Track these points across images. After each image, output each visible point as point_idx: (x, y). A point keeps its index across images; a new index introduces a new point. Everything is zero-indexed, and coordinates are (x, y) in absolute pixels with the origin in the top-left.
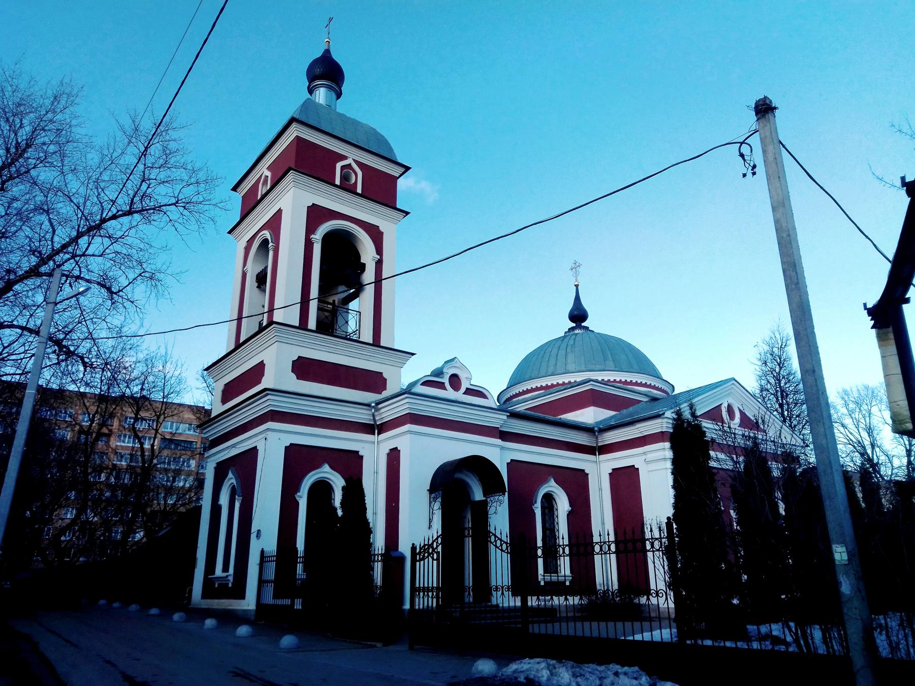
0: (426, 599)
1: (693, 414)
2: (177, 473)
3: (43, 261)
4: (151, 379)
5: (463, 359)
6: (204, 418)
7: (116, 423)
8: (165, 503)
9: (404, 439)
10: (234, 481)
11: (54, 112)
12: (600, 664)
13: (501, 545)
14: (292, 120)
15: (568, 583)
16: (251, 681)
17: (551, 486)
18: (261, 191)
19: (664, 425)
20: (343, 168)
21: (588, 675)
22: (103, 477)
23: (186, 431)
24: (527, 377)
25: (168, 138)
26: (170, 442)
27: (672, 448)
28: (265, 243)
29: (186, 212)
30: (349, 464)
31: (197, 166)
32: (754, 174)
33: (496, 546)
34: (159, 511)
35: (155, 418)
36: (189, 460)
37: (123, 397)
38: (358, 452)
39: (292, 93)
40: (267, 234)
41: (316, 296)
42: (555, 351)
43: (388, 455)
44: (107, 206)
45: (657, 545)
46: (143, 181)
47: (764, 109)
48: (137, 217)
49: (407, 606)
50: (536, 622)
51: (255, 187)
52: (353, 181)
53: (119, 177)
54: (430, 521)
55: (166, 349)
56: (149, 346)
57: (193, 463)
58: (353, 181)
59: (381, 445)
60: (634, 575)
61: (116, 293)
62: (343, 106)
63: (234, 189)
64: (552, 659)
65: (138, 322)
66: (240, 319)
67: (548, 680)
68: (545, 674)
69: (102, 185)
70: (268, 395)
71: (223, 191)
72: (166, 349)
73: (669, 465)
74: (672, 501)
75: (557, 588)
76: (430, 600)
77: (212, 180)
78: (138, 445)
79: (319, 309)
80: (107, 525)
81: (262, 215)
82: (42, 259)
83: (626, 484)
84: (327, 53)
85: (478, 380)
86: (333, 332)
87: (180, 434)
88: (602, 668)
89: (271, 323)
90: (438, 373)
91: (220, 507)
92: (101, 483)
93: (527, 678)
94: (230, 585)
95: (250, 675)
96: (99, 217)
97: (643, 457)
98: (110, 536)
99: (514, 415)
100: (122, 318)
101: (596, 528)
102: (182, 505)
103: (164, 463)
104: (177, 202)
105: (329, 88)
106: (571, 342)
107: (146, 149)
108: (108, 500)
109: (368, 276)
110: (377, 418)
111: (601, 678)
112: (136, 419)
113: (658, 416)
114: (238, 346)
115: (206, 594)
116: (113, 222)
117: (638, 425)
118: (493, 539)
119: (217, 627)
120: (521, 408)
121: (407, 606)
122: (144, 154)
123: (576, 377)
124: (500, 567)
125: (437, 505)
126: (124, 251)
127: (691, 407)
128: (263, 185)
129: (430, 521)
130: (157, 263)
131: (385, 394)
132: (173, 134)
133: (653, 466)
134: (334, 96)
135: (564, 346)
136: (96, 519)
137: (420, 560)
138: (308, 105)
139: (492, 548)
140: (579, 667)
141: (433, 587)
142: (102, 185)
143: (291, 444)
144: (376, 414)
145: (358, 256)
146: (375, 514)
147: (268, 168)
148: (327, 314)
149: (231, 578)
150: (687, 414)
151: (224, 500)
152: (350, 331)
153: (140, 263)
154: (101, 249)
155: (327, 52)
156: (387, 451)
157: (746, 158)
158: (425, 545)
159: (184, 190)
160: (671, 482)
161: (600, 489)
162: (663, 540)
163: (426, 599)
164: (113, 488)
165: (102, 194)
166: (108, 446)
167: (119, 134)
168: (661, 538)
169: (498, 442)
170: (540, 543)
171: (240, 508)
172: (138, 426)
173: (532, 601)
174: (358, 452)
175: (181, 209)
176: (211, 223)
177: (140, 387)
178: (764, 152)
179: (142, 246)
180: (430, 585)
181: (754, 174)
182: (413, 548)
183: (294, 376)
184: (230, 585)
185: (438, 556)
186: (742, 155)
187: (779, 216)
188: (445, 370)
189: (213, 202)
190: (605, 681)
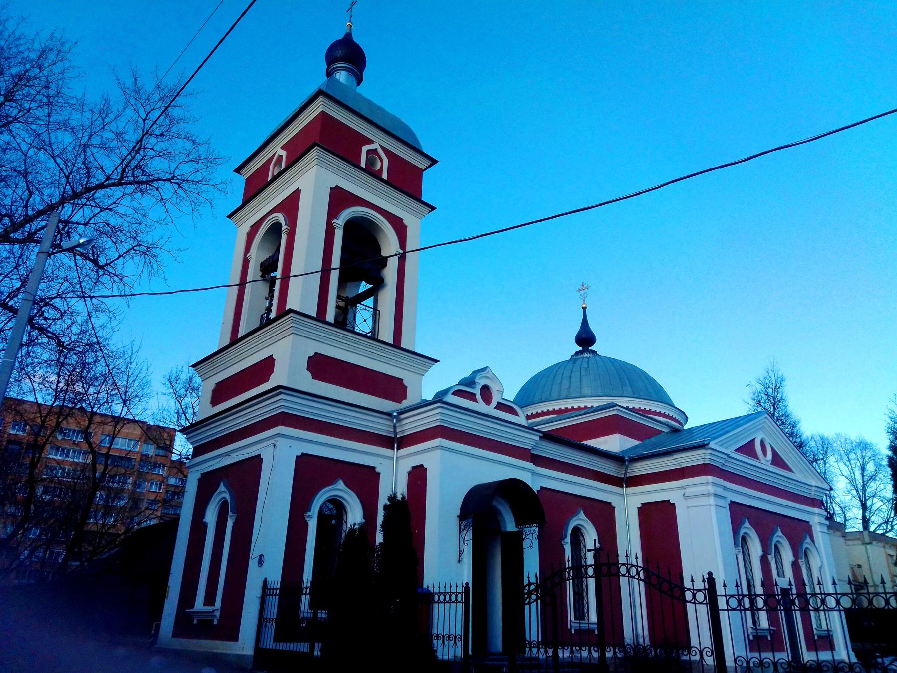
3: (16, 227)
5: (495, 370)
9: (433, 457)
10: (227, 496)
11: (41, 68)
14: (320, 93)
17: (581, 520)
18: (272, 171)
20: (369, 152)
24: (537, 399)
28: (275, 229)
29: (180, 191)
38: (639, 509)
40: (280, 217)
42: (567, 374)
43: (410, 473)
48: (129, 189)
52: (378, 167)
54: (461, 553)
63: (238, 171)
70: (280, 393)
71: (225, 173)
75: (583, 638)
82: (14, 224)
83: (659, 522)
89: (283, 312)
90: (470, 382)
91: (205, 527)
94: (216, 622)
97: (683, 491)
99: (548, 437)
101: (536, 543)
104: (173, 178)
109: (390, 273)
117: (676, 456)
123: (592, 402)
125: (469, 536)
128: (275, 165)
129: (461, 553)
131: (405, 404)
134: (355, 82)
143: (303, 454)
149: (218, 614)
151: (211, 517)
155: (349, 36)
156: (409, 469)
171: (234, 528)
173: (564, 653)
174: (374, 468)
175: (176, 187)
176: (208, 206)
183: (309, 375)
184: (216, 622)
188: (477, 380)
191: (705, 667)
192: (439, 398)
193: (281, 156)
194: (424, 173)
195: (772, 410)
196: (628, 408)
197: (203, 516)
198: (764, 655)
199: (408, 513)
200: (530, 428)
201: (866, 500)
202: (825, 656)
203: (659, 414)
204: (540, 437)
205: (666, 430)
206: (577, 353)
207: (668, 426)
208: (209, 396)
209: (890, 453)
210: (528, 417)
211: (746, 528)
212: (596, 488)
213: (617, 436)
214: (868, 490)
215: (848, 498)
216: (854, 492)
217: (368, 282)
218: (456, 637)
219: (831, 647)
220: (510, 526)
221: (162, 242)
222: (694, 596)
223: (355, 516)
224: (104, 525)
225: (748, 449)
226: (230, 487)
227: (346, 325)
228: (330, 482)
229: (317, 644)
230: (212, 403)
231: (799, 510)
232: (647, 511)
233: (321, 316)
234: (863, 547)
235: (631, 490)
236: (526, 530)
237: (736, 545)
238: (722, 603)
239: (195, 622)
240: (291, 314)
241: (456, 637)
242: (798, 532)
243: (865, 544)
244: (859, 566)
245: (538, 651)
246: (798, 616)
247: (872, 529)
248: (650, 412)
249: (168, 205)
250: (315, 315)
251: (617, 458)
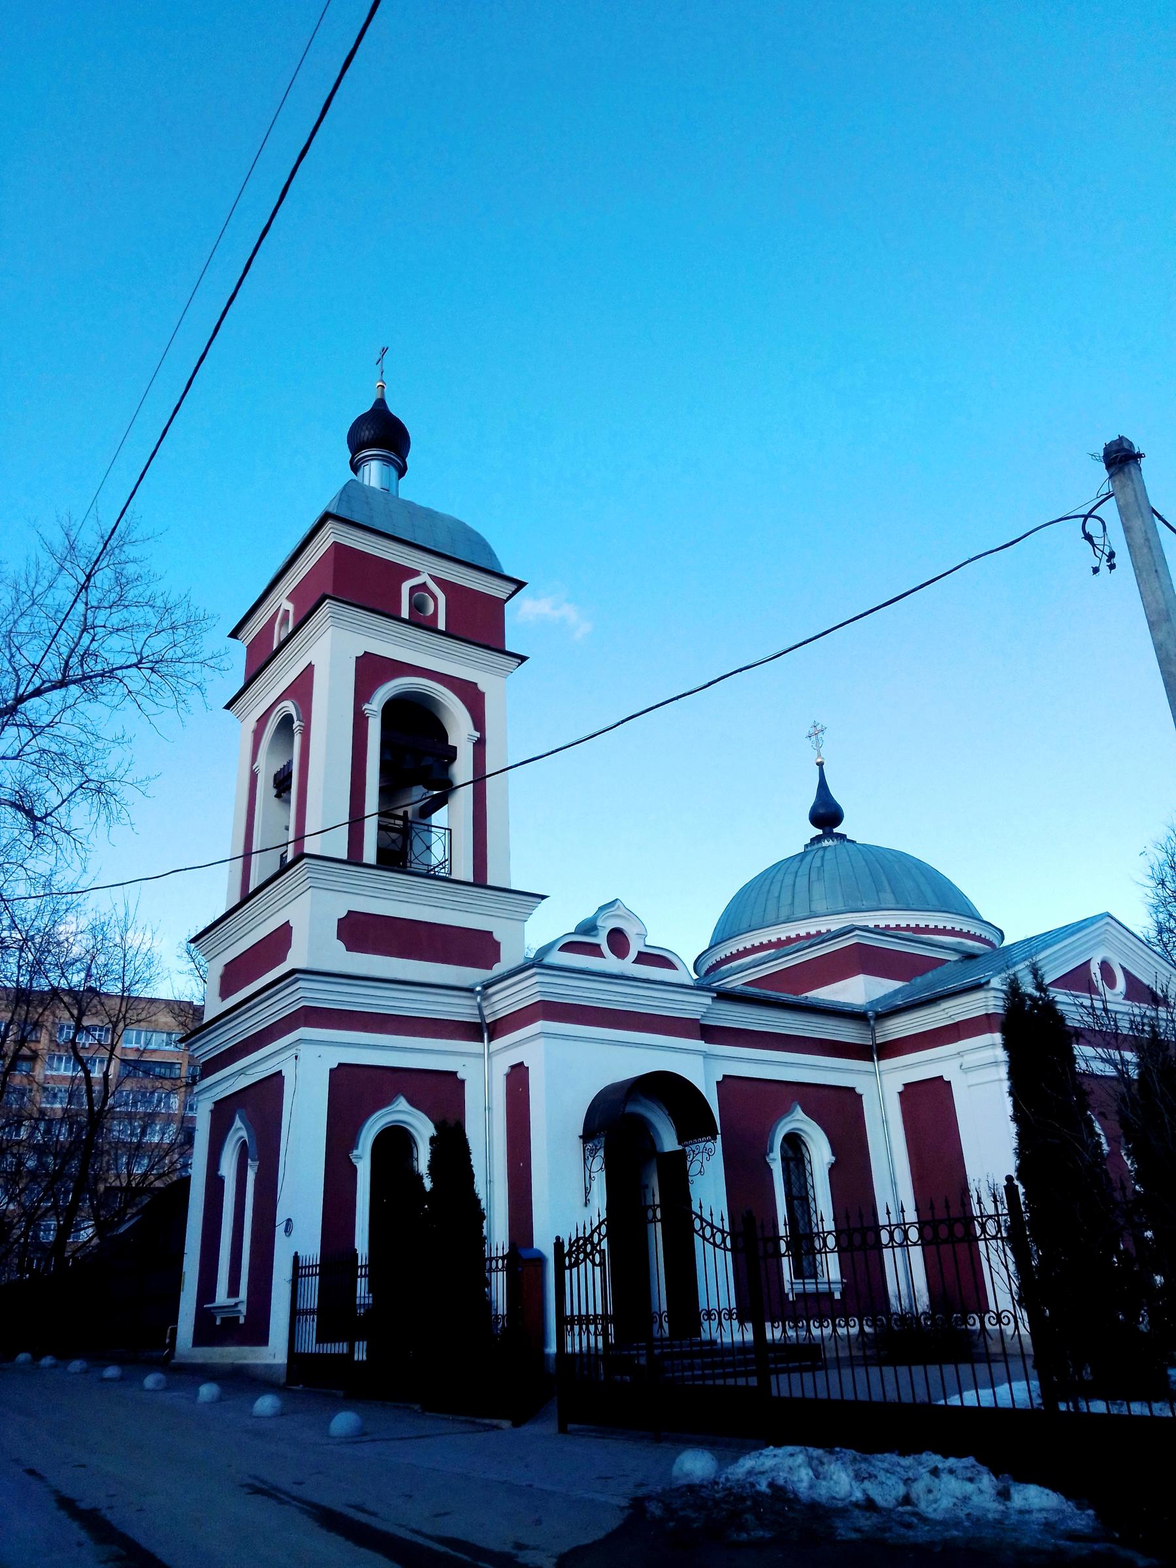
0: (584, 1338)
1: (1040, 987)
2: (149, 1119)
4: (101, 959)
5: (630, 902)
6: (191, 1022)
7: (44, 1038)
8: (130, 1174)
10: (244, 1133)
12: (904, 1453)
13: (713, 1235)
14: (327, 517)
15: (837, 1296)
16: (281, 1502)
17: (797, 1120)
18: (278, 635)
19: (989, 1002)
20: (413, 590)
21: (882, 1476)
22: (24, 1134)
23: (160, 1044)
24: (744, 926)
25: (123, 557)
26: (137, 1066)
27: (1007, 1046)
28: (287, 721)
29: (155, 677)
30: (442, 1094)
31: (172, 600)
32: (1112, 567)
33: (703, 1237)
34: (120, 1189)
35: (110, 1026)
36: (168, 1096)
37: (55, 992)
39: (323, 470)
40: (289, 706)
41: (375, 809)
42: (789, 880)
43: (508, 1076)
44: (25, 675)
45: (991, 1228)
46: (83, 632)
47: (1121, 458)
48: (74, 689)
49: (552, 1349)
50: (783, 1371)
51: (269, 628)
52: (431, 610)
53: (44, 626)
54: (587, 1191)
55: (127, 907)
56: (97, 907)
57: (175, 1102)
58: (431, 610)
59: (495, 1059)
60: (956, 1282)
61: (40, 819)
62: (410, 489)
63: (234, 634)
64: (817, 1446)
65: (77, 865)
66: (247, 855)
67: (811, 1487)
68: (805, 1474)
69: (17, 641)
70: (298, 980)
71: (216, 639)
72: (127, 907)
73: (1003, 1072)
74: (1014, 1143)
75: (818, 1306)
76: (592, 1339)
77: (198, 621)
78: (81, 1074)
79: (381, 827)
80: (32, 1217)
81: (282, 675)
83: (928, 1107)
84: (380, 405)
85: (657, 938)
86: (405, 866)
87: (154, 1051)
88: (907, 1461)
89: (300, 856)
90: (588, 927)
91: (221, 1181)
92: (19, 1143)
93: (771, 1485)
94: (242, 1321)
95: (277, 1489)
96: (12, 694)
98: (36, 1236)
99: (725, 996)
100: (52, 860)
101: (883, 1197)
102: (159, 1177)
103: (126, 1104)
104: (140, 662)
105: (386, 460)
106: (817, 863)
107: (89, 577)
108: (33, 1175)
109: (462, 770)
110: (486, 1012)
111: (907, 1481)
112: (79, 1028)
113: (978, 987)
114: (246, 898)
116: (35, 701)
117: (945, 1005)
118: (697, 1224)
119: (221, 1399)
120: (735, 982)
121: (552, 1349)
122: (84, 587)
124: (716, 1275)
125: (598, 1163)
126: (54, 748)
127: (1035, 971)
128: (281, 625)
129: (587, 1191)
130: (110, 763)
131: (498, 969)
132: (131, 551)
133: (974, 1078)
134: (394, 473)
135: (804, 869)
136: (11, 1207)
137: (571, 1267)
138: (349, 492)
139: (698, 1240)
140: (866, 1460)
141: (596, 1316)
142: (17, 641)
143: (340, 1065)
144: (484, 1004)
145: (444, 736)
146: (489, 1182)
147: (289, 598)
148: (394, 835)
149: (243, 1308)
150: (1029, 988)
151: (228, 1168)
152: (434, 862)
153: (81, 766)
154: (17, 746)
155: (381, 403)
156: (506, 1070)
157: (1096, 541)
158: (578, 1239)
159: (151, 641)
160: (1010, 1110)
161: (885, 1122)
162: (1002, 1219)
163: (584, 1338)
164: (40, 1150)
165: (18, 656)
166: (30, 1077)
167: (45, 557)
168: (998, 1215)
169: (700, 1045)
170: (782, 1231)
172: (83, 1040)
173: (773, 1333)
174: (455, 1073)
175: (147, 672)
177: (83, 975)
178: (1127, 530)
179: (83, 738)
180: (591, 1312)
181: (1112, 567)
182: (559, 1245)
184: (242, 1321)
185: (603, 1258)
186: (1088, 537)
187: (1161, 636)
188: (599, 923)
189: (201, 658)
190: (915, 1485)
204: (713, 998)
205: (953, 957)
206: (817, 840)
212: (826, 1069)
213: (861, 978)
218: (719, 1313)
221: (120, 772)
228: (384, 1101)
230: (221, 995)
235: (886, 1064)
236: (693, 1147)
239: (218, 1322)
240: (305, 860)
241: (719, 1313)
250: (345, 856)
251: (855, 1016)
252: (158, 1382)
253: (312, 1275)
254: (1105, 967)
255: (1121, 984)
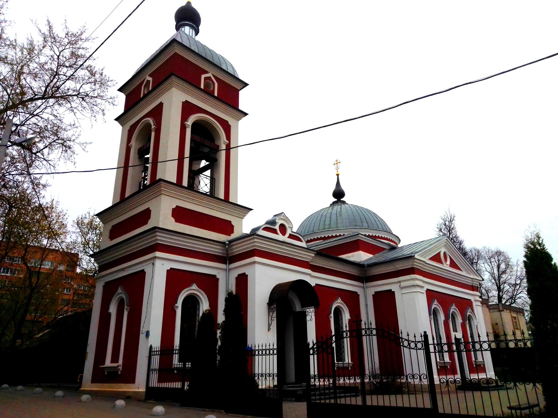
17: (338, 303)
29: (84, 103)
38: (245, 273)
40: (151, 120)
45: (485, 346)
48: (52, 101)
54: (269, 325)
83: (386, 303)
90: (273, 222)
91: (109, 315)
94: (119, 373)
97: (399, 284)
101: (314, 317)
104: (78, 94)
110: (229, 252)
115: (95, 380)
118: (406, 343)
123: (346, 232)
133: (404, 291)
149: (121, 368)
151: (113, 309)
175: (81, 99)
183: (173, 220)
184: (119, 373)
191: (423, 386)
192: (254, 232)
193: (148, 81)
194: (240, 92)
195: (448, 234)
196: (365, 235)
197: (108, 308)
198: (449, 377)
199: (238, 302)
200: (308, 249)
201: (500, 285)
202: (482, 376)
203: (384, 239)
204: (315, 254)
206: (334, 203)
207: (389, 245)
208: (107, 233)
209: (525, 259)
210: (308, 242)
211: (435, 305)
214: (502, 280)
215: (490, 284)
216: (493, 281)
217: (207, 161)
218: (273, 375)
219: (484, 370)
220: (298, 308)
222: (416, 345)
223: (205, 306)
224: (35, 316)
225: (436, 258)
226: (126, 289)
227: (194, 188)
228: (189, 285)
229: (186, 383)
230: (110, 238)
231: (467, 293)
232: (378, 296)
233: (179, 183)
234: (498, 313)
235: (369, 284)
236: (308, 310)
237: (430, 314)
238: (432, 348)
239: (106, 373)
241: (273, 375)
242: (465, 305)
243: (500, 311)
244: (497, 324)
245: (315, 380)
246: (464, 354)
247: (503, 302)
248: (378, 237)
249: (75, 110)
250: (175, 182)
252: (88, 399)
253: (156, 355)
254: (445, 254)
255: (448, 262)
